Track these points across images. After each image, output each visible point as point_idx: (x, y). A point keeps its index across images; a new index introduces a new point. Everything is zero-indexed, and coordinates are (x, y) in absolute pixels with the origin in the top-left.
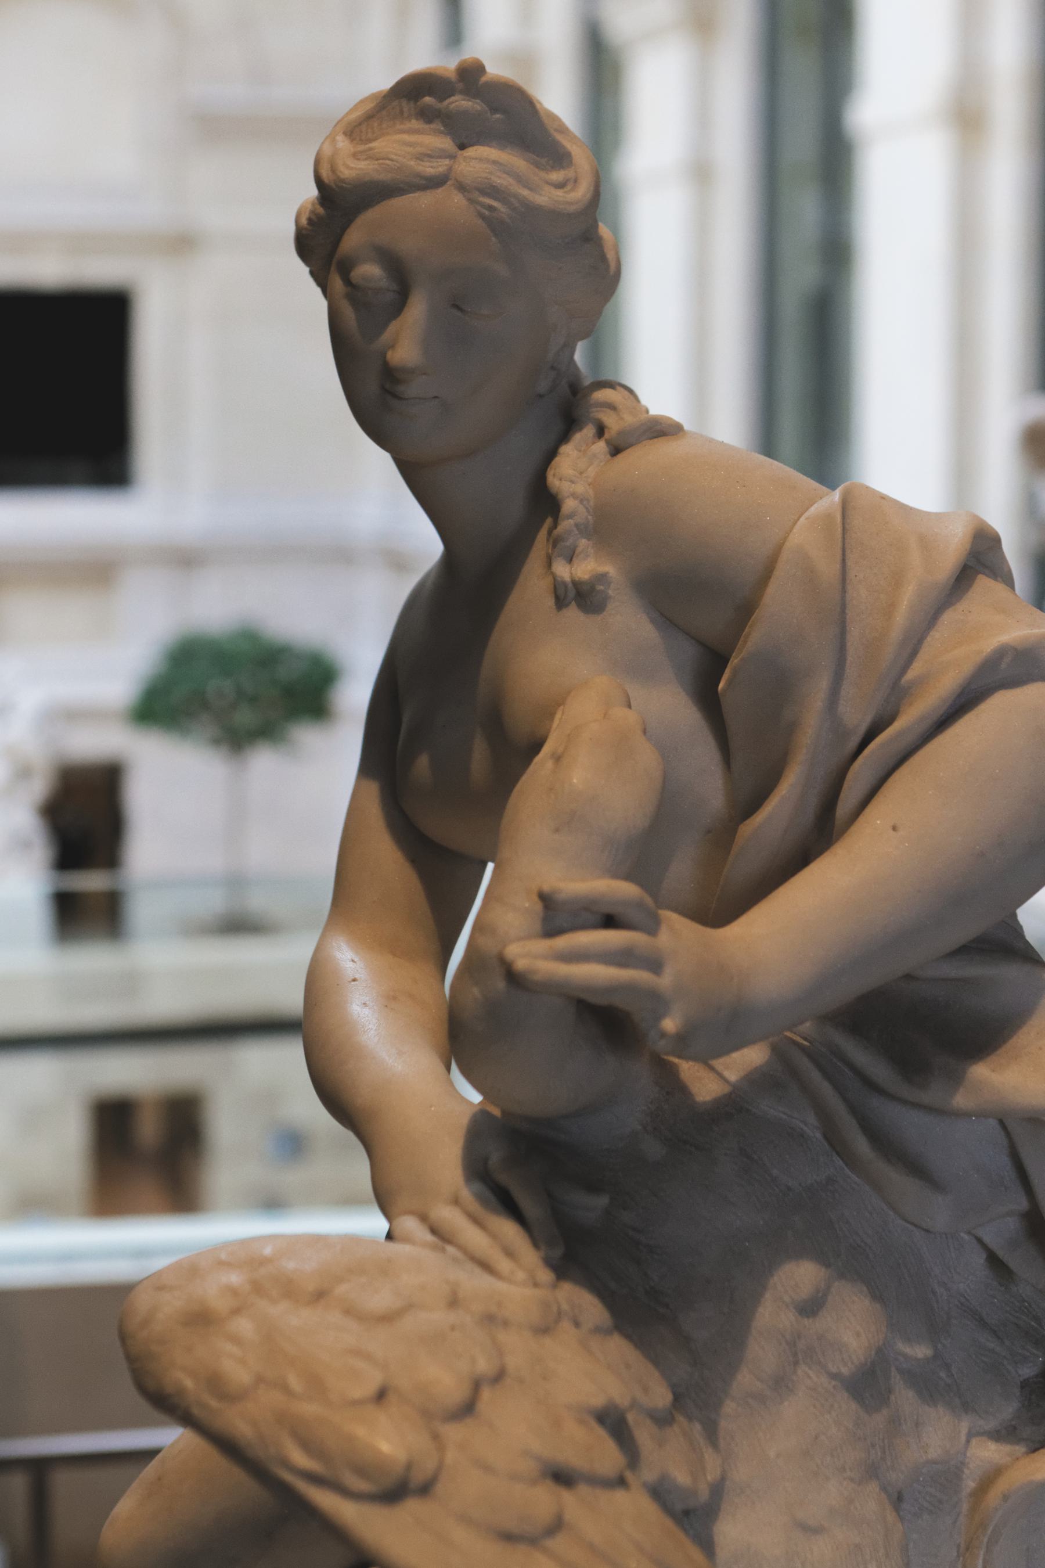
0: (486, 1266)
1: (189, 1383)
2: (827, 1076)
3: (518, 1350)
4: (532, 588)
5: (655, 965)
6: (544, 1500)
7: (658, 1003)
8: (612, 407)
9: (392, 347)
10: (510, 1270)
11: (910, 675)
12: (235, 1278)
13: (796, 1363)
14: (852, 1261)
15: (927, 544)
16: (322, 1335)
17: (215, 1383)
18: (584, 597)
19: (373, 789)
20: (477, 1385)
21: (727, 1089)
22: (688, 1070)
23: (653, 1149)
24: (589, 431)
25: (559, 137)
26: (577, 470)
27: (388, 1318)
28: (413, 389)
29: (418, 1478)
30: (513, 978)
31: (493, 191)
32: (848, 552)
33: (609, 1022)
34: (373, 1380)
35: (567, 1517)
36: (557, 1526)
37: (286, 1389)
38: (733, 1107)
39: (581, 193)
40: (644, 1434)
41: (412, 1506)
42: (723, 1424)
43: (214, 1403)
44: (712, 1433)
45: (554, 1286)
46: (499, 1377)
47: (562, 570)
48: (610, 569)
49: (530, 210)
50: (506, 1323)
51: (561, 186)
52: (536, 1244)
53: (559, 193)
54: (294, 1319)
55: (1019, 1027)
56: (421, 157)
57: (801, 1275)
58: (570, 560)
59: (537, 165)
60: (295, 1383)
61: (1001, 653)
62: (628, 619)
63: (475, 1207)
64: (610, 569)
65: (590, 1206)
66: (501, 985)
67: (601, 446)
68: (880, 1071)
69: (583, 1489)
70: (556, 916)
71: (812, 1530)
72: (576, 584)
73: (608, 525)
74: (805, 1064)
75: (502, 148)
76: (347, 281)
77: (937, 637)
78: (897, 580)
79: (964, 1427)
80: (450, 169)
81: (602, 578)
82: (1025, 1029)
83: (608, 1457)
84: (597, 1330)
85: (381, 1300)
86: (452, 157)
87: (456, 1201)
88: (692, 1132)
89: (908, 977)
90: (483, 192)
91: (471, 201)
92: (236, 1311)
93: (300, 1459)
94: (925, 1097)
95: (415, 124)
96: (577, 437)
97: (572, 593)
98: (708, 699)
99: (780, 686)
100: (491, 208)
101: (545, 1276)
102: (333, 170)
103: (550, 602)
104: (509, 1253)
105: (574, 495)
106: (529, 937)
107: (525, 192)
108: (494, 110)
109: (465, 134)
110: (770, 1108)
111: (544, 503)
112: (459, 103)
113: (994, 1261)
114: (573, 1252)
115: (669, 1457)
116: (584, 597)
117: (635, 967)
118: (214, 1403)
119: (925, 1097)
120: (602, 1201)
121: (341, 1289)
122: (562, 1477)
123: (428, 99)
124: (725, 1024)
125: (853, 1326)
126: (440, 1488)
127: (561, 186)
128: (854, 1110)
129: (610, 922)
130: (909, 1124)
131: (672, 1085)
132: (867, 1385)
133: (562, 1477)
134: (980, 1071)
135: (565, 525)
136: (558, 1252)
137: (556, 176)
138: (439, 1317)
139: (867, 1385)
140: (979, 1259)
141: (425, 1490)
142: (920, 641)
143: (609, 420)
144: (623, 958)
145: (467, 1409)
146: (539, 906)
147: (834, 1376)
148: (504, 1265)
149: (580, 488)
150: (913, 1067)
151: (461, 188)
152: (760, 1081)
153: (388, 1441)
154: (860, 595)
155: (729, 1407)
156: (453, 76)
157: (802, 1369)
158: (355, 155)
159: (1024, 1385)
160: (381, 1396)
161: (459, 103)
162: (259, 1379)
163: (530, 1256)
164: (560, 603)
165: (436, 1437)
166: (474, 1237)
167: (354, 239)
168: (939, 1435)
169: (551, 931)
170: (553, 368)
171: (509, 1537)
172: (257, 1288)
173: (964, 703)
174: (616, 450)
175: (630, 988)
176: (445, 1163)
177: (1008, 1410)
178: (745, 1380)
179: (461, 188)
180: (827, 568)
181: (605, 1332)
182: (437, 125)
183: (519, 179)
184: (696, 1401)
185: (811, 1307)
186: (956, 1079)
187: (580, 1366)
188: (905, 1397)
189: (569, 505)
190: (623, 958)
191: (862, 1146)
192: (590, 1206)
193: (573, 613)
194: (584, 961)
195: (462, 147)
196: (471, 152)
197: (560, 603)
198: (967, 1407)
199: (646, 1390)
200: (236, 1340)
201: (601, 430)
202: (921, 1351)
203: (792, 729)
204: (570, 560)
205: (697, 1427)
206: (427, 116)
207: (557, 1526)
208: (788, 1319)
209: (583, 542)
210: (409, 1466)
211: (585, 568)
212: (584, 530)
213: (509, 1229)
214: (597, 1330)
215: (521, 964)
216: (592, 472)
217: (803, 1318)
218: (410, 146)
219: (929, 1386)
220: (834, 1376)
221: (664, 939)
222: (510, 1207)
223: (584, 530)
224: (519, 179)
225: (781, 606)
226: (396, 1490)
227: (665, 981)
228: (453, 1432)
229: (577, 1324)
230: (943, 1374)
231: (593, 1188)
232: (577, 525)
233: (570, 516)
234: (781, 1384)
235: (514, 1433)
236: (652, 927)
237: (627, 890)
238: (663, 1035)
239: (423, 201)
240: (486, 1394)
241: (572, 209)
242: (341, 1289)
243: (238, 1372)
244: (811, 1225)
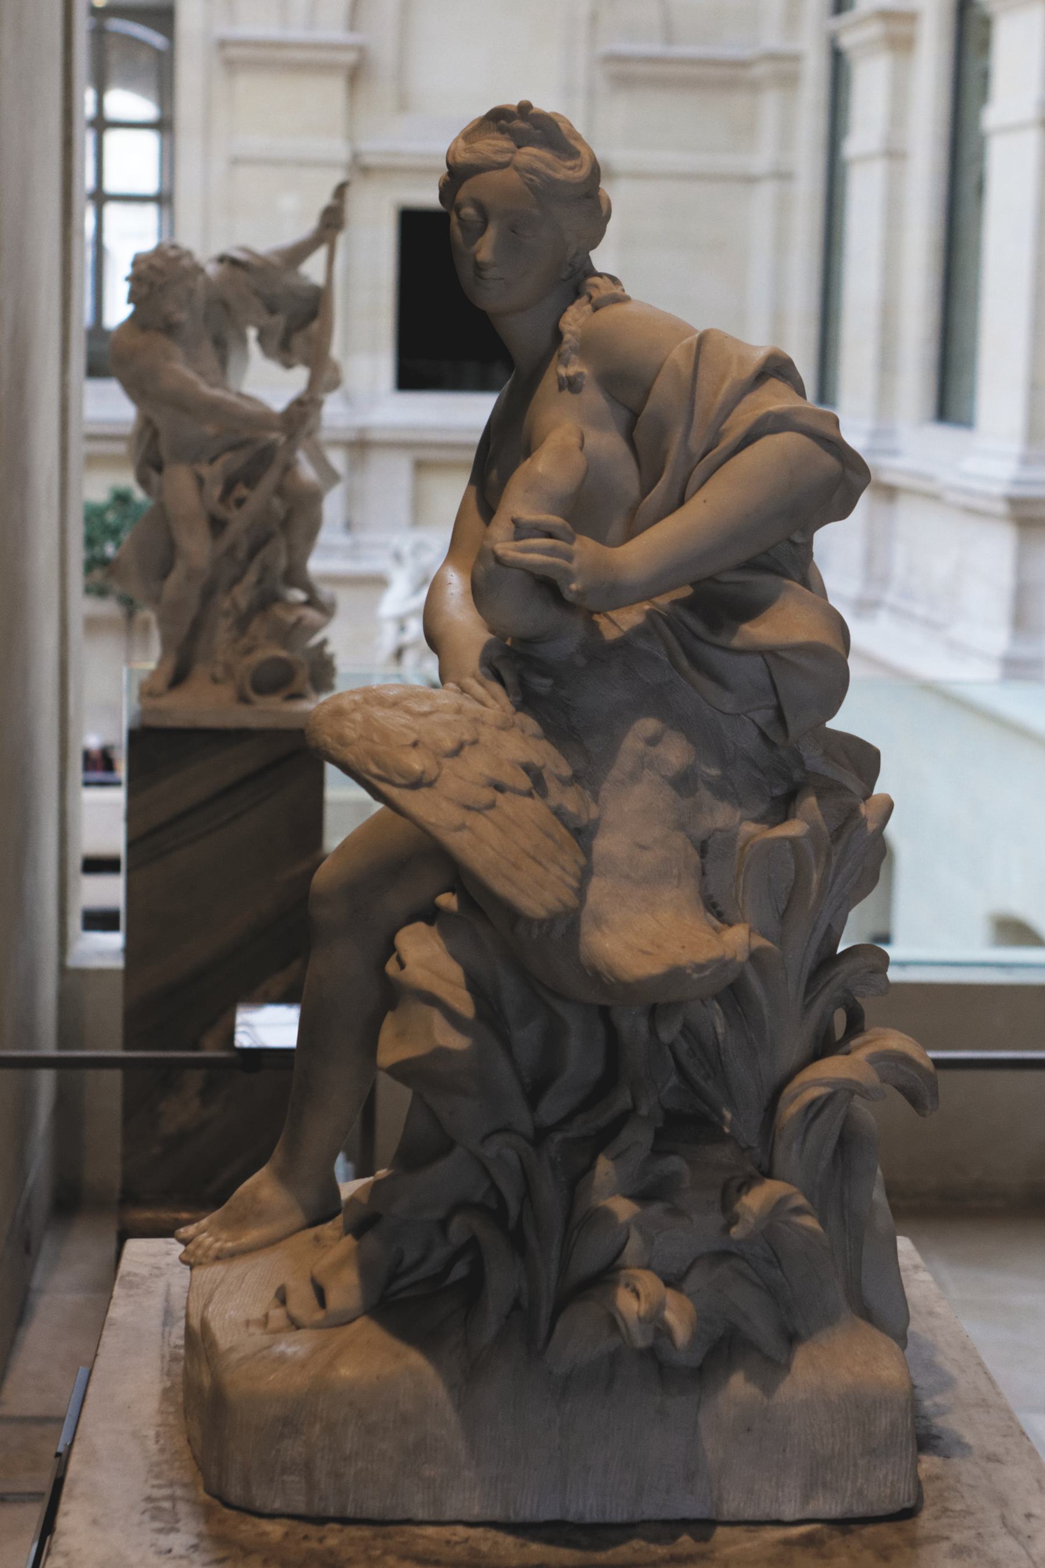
0: (482, 703)
1: (329, 739)
2: (671, 629)
3: (486, 735)
4: (549, 383)
5: (569, 558)
6: (487, 795)
7: (569, 576)
8: (596, 286)
9: (478, 251)
10: (495, 703)
11: (723, 427)
12: (357, 698)
13: (643, 768)
14: (678, 721)
15: (742, 361)
16: (395, 720)
17: (341, 740)
18: (571, 385)
19: (474, 489)
20: (461, 746)
21: (621, 634)
22: (602, 621)
23: (580, 661)
24: (585, 298)
25: (572, 142)
26: (575, 319)
27: (425, 715)
28: (490, 273)
29: (427, 778)
30: (498, 560)
31: (533, 171)
32: (701, 366)
33: (547, 586)
34: (413, 737)
35: (497, 804)
36: (492, 805)
37: (373, 741)
38: (624, 644)
39: (584, 172)
40: (552, 786)
41: (424, 790)
42: (602, 794)
43: (339, 747)
44: (596, 796)
45: (515, 714)
46: (475, 742)
47: (562, 371)
48: (585, 371)
49: (553, 182)
50: (483, 723)
51: (572, 168)
52: (508, 695)
53: (571, 172)
54: (379, 713)
55: (769, 606)
56: (496, 152)
57: (649, 725)
58: (566, 366)
59: (559, 158)
60: (376, 737)
61: (769, 415)
62: (593, 397)
63: (482, 678)
64: (585, 371)
65: (542, 684)
66: (492, 564)
67: (589, 307)
68: (699, 627)
69: (508, 794)
70: (521, 530)
71: (643, 848)
72: (568, 377)
73: (587, 348)
74: (661, 623)
75: (540, 148)
76: (459, 217)
77: (741, 407)
78: (722, 379)
79: (739, 814)
80: (512, 159)
81: (580, 374)
82: (772, 608)
83: (525, 782)
84: (534, 736)
85: (425, 708)
86: (514, 152)
87: (474, 676)
88: (601, 654)
89: (711, 579)
90: (527, 172)
91: (522, 176)
92: (353, 710)
93: (375, 769)
94: (721, 640)
95: (497, 134)
96: (578, 302)
97: (566, 383)
98: (630, 439)
99: (662, 432)
100: (531, 180)
101: (510, 708)
102: (454, 158)
103: (556, 387)
104: (494, 698)
105: (570, 332)
106: (508, 541)
107: (550, 172)
108: (536, 128)
109: (521, 140)
110: (643, 645)
111: (558, 336)
112: (518, 124)
113: (763, 735)
114: (527, 701)
115: (570, 800)
116: (571, 385)
117: (556, 557)
118: (339, 747)
119: (721, 640)
120: (548, 682)
121: (405, 703)
122: (499, 787)
123: (503, 122)
124: (616, 594)
125: (675, 753)
126: (437, 785)
127: (572, 168)
128: (683, 646)
129: (550, 535)
130: (716, 658)
131: (594, 629)
132: (683, 783)
133: (499, 787)
134: (746, 628)
135: (565, 347)
136: (519, 699)
137: (569, 163)
138: (449, 717)
139: (683, 783)
140: (755, 733)
141: (430, 784)
142: (732, 410)
143: (595, 294)
144: (551, 552)
145: (457, 752)
146: (513, 526)
147: (663, 777)
148: (491, 702)
149: (573, 328)
150: (714, 625)
151: (517, 169)
152: (640, 631)
153: (416, 763)
154: (704, 385)
155: (606, 785)
156: (515, 110)
157: (646, 771)
158: (465, 150)
159: (773, 798)
160: (415, 744)
161: (518, 124)
162: (361, 737)
163: (504, 699)
164: (561, 388)
165: (438, 764)
166: (479, 690)
167: (463, 194)
168: (722, 816)
169: (518, 538)
170: (570, 265)
171: (468, 808)
172: (366, 701)
173: (748, 439)
174: (596, 309)
175: (552, 566)
176: (471, 659)
177: (762, 808)
178: (615, 773)
179: (517, 169)
180: (686, 371)
181: (539, 738)
182: (507, 136)
183: (548, 165)
184: (587, 777)
185: (653, 741)
186: (734, 632)
187: (520, 744)
188: (705, 794)
189: (567, 337)
190: (551, 552)
191: (685, 663)
192: (542, 684)
193: (566, 393)
194: (534, 553)
195: (519, 147)
196: (524, 150)
197: (561, 388)
198: (740, 805)
199: (557, 767)
200: (353, 721)
201: (591, 297)
202: (715, 772)
203: (666, 453)
204: (566, 366)
205: (588, 793)
206: (502, 130)
207: (492, 805)
208: (640, 745)
209: (573, 356)
210: (423, 772)
211: (572, 370)
212: (574, 350)
213: (496, 688)
214: (534, 736)
215: (500, 552)
216: (582, 320)
217: (651, 751)
218: (493, 146)
219: (721, 791)
220: (663, 777)
221: (576, 546)
222: (499, 679)
223: (574, 350)
224: (548, 165)
225: (664, 390)
226: (417, 783)
227: (574, 566)
228: (447, 762)
229: (523, 731)
230: (729, 787)
231: (545, 675)
232: (570, 348)
233: (567, 342)
234: (634, 777)
235: (477, 765)
236: (571, 542)
237: (556, 520)
238: (571, 591)
239: (496, 176)
240: (467, 748)
241: (578, 180)
242: (405, 703)
243: (351, 733)
244: (658, 702)
